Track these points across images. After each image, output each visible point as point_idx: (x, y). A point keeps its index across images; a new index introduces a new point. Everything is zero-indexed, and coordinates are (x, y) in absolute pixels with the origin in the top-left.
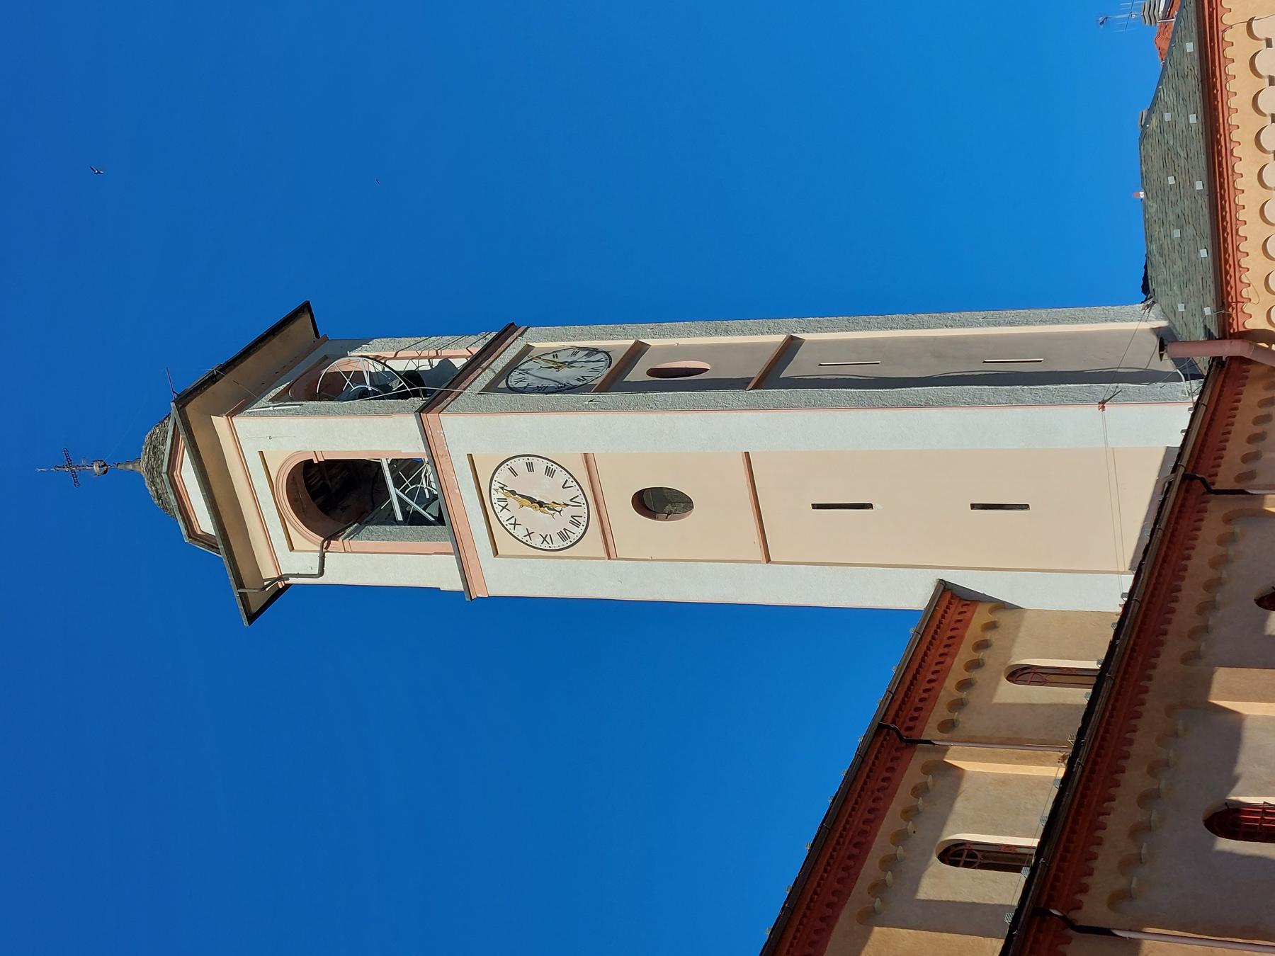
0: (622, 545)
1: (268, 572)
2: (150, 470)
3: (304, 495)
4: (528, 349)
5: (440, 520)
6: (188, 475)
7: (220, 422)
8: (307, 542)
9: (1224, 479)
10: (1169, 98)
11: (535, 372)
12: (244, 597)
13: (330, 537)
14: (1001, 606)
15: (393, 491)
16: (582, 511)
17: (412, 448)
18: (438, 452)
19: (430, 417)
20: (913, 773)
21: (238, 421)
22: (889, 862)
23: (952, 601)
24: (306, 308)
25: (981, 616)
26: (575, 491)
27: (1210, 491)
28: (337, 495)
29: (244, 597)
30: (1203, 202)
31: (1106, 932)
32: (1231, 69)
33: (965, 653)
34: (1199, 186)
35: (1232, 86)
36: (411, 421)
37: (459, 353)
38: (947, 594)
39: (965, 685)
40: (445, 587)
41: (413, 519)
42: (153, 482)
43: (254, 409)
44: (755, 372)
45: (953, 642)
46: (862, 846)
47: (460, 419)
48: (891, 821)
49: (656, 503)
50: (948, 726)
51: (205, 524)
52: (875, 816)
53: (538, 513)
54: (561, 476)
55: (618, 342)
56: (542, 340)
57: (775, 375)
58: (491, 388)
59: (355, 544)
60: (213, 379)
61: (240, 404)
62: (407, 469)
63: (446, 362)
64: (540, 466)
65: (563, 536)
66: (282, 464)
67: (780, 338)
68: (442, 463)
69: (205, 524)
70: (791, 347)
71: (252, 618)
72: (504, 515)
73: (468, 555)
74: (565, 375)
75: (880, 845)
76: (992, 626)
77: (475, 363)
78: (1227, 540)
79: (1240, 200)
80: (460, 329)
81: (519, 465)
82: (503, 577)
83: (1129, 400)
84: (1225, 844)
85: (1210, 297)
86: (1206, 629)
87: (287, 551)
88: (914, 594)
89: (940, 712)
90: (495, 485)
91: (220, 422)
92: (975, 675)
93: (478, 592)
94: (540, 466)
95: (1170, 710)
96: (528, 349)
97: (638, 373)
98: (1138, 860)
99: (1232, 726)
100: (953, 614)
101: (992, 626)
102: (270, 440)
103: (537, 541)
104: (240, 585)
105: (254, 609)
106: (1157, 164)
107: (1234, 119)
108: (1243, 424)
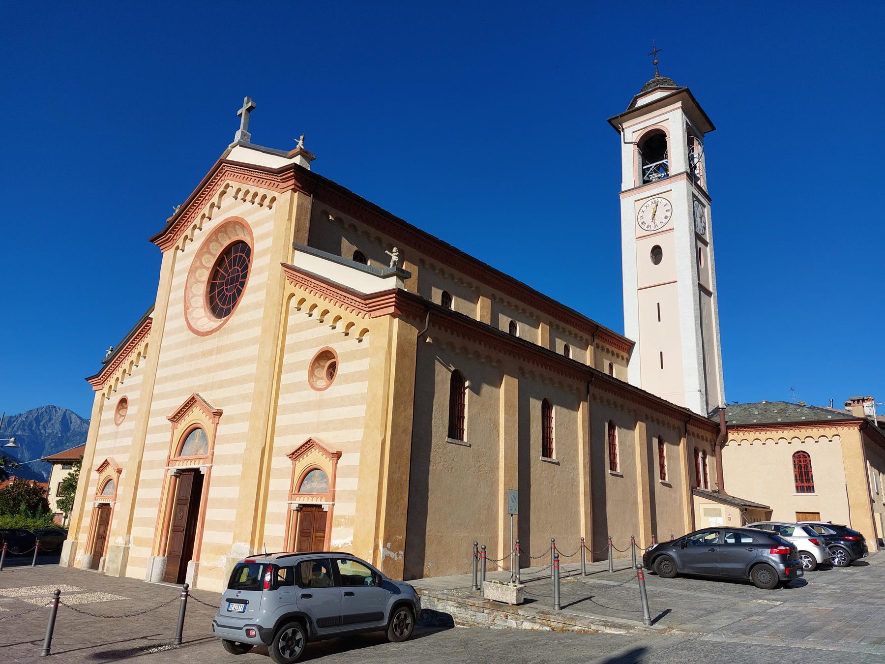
0: (640, 242)
1: (625, 125)
2: (658, 81)
3: (652, 134)
4: (704, 206)
5: (645, 182)
6: (658, 95)
7: (679, 104)
8: (636, 137)
9: (689, 427)
10: (806, 411)
11: (699, 209)
12: (617, 117)
13: (638, 145)
14: (628, 361)
15: (654, 164)
16: (652, 228)
17: (672, 171)
18: (672, 179)
19: (685, 176)
20: (586, 336)
21: (680, 110)
22: (564, 330)
23: (629, 346)
24: (714, 128)
25: (626, 355)
26: (660, 226)
27: (686, 423)
28: (653, 146)
29: (617, 117)
30: (772, 421)
31: (588, 393)
32: (821, 430)
33: (616, 351)
34: (779, 420)
35: (815, 430)
36: (683, 170)
37: (702, 183)
38: (629, 346)
39: (608, 351)
40: (623, 185)
41: (644, 170)
42: (654, 82)
43: (685, 117)
44: (701, 282)
45: (619, 347)
46: (567, 322)
47: (685, 186)
48: (575, 330)
49: (657, 253)
50: (597, 346)
51: (641, 102)
52: (575, 326)
53: (651, 215)
54: (665, 221)
55: (708, 237)
56: (707, 211)
57: (703, 289)
58: (694, 196)
59: (636, 153)
60: (694, 100)
61: (685, 110)
62: (665, 168)
63: (698, 179)
64: (668, 214)
65: (643, 223)
66: (663, 126)
67: (711, 290)
68: (668, 181)
69: (641, 102)
70: (709, 294)
71: (609, 121)
72: (649, 203)
73: (635, 191)
74: (698, 220)
75: (568, 327)
76: (623, 359)
77: (699, 188)
78: (674, 428)
79: (774, 432)
80: (708, 183)
81: (669, 207)
82: (628, 206)
83: (701, 398)
84: (607, 425)
85: (738, 423)
86: (653, 421)
87: (633, 131)
88: (630, 333)
89: (601, 344)
90: (660, 200)
91: (679, 104)
92: (610, 354)
93: (621, 196)
94: (668, 214)
95: (635, 410)
96: (704, 206)
97: (700, 245)
98: (602, 402)
99: (632, 428)
100: (626, 347)
101: (623, 359)
102: (673, 122)
103: (641, 214)
104: (621, 116)
105: (613, 122)
106: (779, 407)
107: (803, 430)
108: (702, 432)
